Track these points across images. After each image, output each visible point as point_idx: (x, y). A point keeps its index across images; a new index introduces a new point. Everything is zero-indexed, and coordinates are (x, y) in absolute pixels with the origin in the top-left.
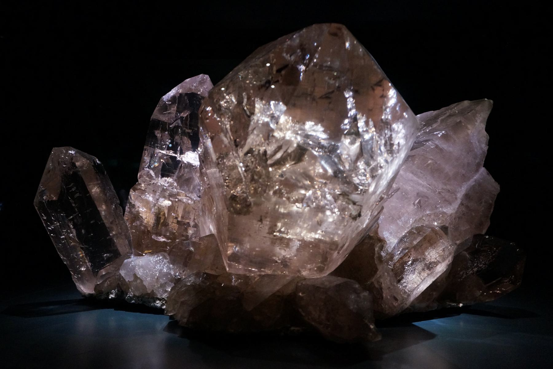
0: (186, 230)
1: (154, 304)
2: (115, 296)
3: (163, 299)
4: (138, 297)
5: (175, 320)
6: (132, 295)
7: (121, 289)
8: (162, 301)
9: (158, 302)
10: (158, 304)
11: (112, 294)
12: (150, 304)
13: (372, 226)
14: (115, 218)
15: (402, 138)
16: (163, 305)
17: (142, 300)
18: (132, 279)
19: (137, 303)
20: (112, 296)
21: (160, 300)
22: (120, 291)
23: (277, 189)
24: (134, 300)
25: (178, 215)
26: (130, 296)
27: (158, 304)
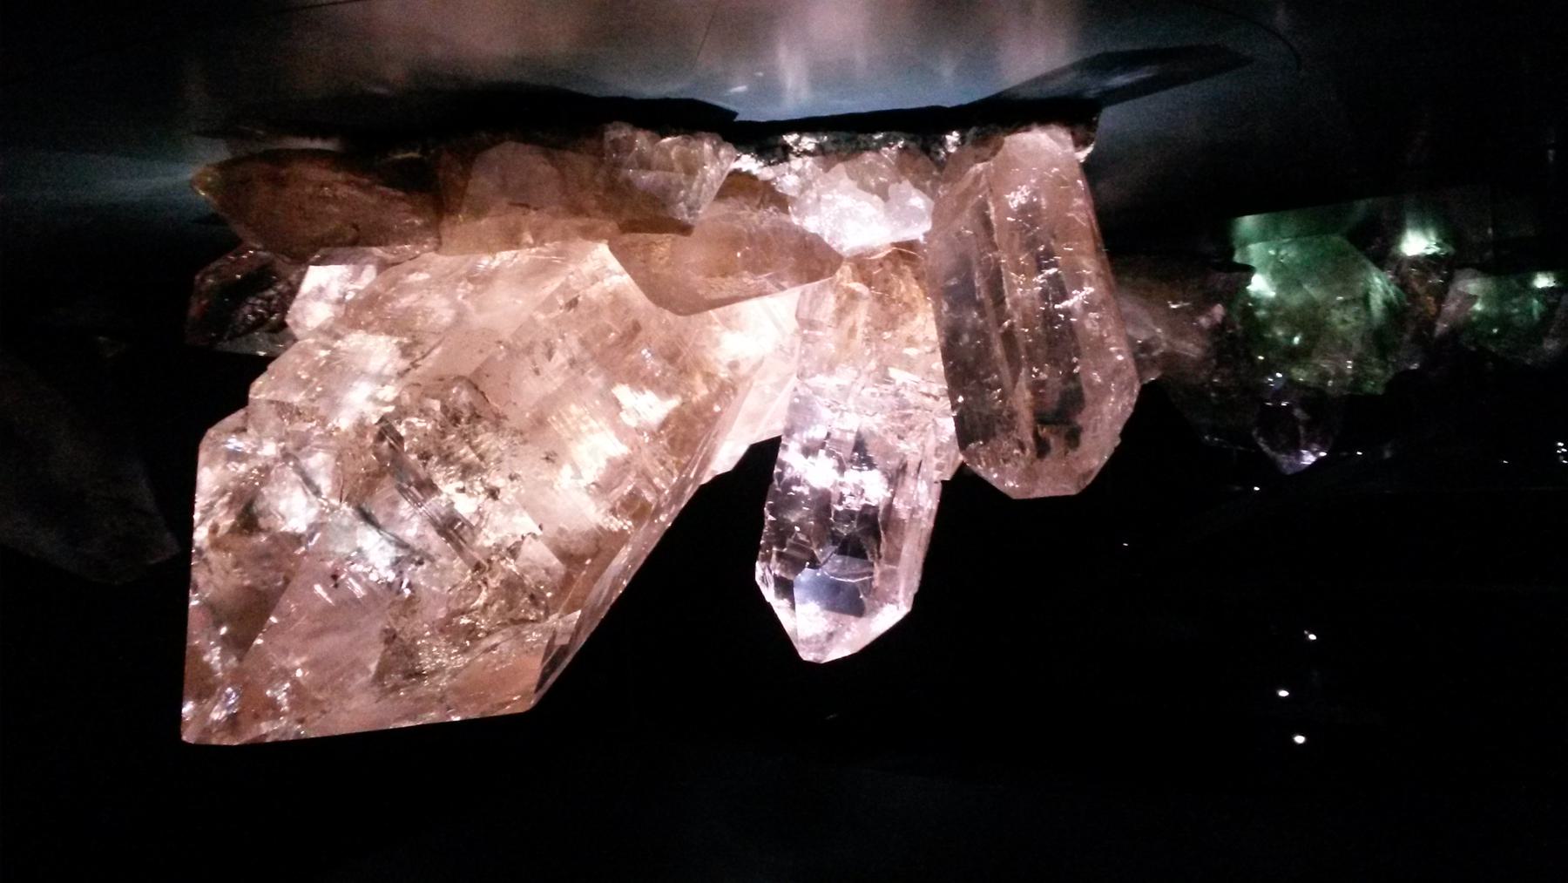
0: (979, 313)
1: (818, 140)
2: (945, 139)
3: (798, 156)
4: (867, 149)
5: (395, 340)
6: (885, 152)
7: (932, 159)
8: (801, 150)
9: (811, 147)
10: (808, 143)
11: (955, 144)
12: (832, 139)
13: (1291, 48)
14: (641, 341)
15: (468, 195)
16: (797, 143)
17: (858, 143)
18: (892, 189)
19: (869, 135)
20: (953, 137)
21: (806, 152)
22: (932, 154)
23: (199, 194)
24: (876, 141)
25: (800, 361)
26: (887, 149)
27: (810, 143)
